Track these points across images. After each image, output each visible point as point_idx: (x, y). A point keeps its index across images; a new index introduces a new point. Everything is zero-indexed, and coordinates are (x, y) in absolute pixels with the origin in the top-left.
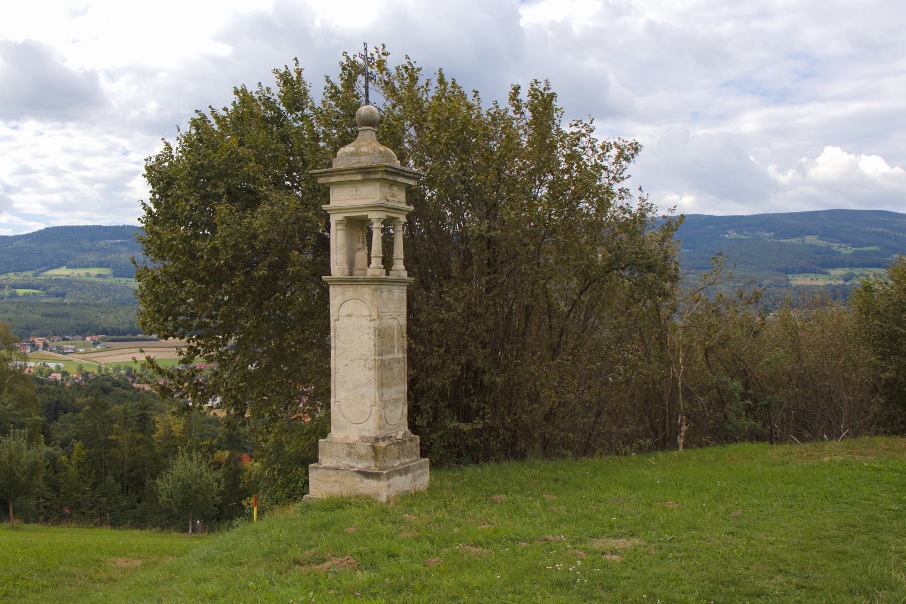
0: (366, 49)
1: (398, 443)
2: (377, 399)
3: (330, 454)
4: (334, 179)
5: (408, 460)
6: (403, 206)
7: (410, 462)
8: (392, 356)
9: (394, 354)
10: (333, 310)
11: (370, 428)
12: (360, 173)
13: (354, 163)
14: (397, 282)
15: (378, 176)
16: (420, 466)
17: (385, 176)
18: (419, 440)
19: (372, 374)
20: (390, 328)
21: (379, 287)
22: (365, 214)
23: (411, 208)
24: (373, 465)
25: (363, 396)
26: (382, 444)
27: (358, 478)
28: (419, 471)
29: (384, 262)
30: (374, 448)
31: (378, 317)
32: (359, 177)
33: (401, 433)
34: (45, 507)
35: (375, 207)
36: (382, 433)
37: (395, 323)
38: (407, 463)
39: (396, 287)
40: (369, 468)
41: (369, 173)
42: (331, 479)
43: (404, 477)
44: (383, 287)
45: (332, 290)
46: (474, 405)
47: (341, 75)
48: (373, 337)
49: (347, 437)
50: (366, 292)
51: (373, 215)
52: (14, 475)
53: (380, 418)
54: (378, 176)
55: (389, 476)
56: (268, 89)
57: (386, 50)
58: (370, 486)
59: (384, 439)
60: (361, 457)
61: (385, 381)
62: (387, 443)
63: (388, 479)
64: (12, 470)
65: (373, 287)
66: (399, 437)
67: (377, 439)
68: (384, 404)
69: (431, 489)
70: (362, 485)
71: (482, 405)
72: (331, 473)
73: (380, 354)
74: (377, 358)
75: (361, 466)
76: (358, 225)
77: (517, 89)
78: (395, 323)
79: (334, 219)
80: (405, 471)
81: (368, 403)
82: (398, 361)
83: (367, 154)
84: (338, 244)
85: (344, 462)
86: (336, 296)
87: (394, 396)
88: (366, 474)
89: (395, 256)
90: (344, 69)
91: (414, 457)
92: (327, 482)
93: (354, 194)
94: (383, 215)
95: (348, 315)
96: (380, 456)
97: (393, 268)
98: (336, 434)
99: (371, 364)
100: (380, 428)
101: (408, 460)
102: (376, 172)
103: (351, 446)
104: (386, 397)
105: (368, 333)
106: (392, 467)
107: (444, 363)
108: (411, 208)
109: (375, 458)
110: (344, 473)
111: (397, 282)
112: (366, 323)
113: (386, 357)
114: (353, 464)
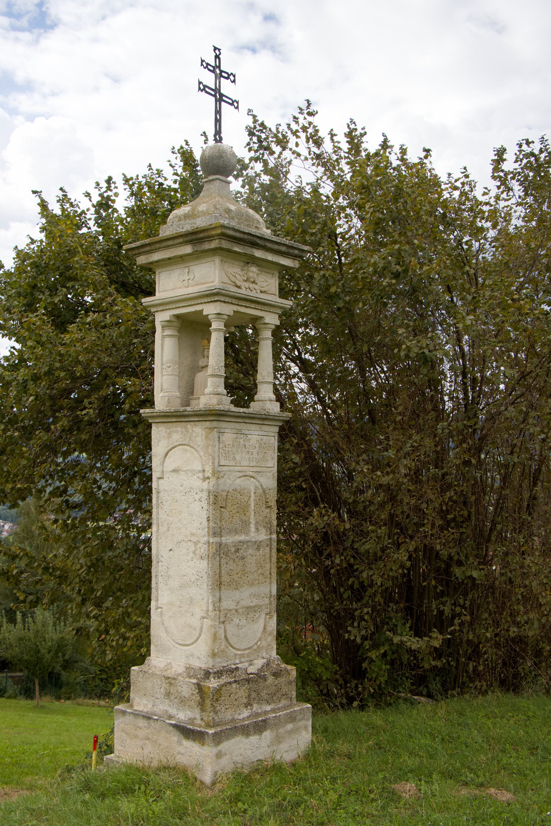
0: (217, 57)
1: (248, 681)
2: (211, 608)
3: (147, 688)
4: (156, 257)
5: (268, 708)
6: (275, 299)
7: (273, 711)
8: (243, 537)
9: (247, 533)
10: (155, 463)
11: (200, 656)
12: (190, 242)
13: (187, 227)
14: (264, 419)
15: (214, 245)
16: (292, 718)
17: (225, 244)
18: (294, 673)
19: (204, 565)
20: (241, 492)
21: (215, 424)
22: (198, 308)
23: (288, 303)
24: (198, 717)
25: (191, 601)
26: (213, 683)
27: (175, 737)
28: (290, 726)
29: (231, 388)
30: (200, 688)
31: (214, 474)
32: (188, 249)
33: (259, 663)
34: (102, 680)
35: (213, 296)
36: (220, 663)
37: (251, 485)
38: (266, 713)
39: (253, 427)
40: (192, 721)
41: (201, 241)
42: (142, 733)
43: (254, 739)
44: (224, 425)
45: (155, 431)
46: (447, 610)
47: (248, 144)
48: (206, 507)
49: (169, 666)
50: (198, 431)
51: (209, 310)
52: (39, 651)
53: (215, 637)
54: (214, 245)
55: (218, 738)
56: (159, 173)
57: (312, 108)
58: (189, 753)
59: (219, 674)
60: (183, 702)
61: (225, 578)
62: (224, 679)
63: (218, 743)
64: (37, 646)
65: (208, 424)
66: (252, 669)
67: (207, 674)
68: (223, 616)
69: (311, 756)
70: (181, 749)
71: (458, 609)
72: (142, 723)
73: (217, 532)
74: (211, 540)
75: (182, 716)
76: (193, 328)
77: (501, 153)
78: (251, 485)
79: (161, 318)
80: (259, 727)
81: (199, 612)
82: (258, 545)
83: (204, 213)
84: (165, 359)
85: (163, 706)
86: (161, 438)
87: (244, 603)
88: (187, 732)
89: (259, 378)
90: (251, 134)
91: (284, 702)
92: (136, 736)
93: (186, 277)
94: (228, 310)
95: (175, 471)
96: (208, 702)
97: (256, 397)
98: (157, 660)
99: (203, 549)
100: (214, 655)
101: (268, 708)
102: (210, 238)
103: (170, 681)
104: (225, 604)
105: (200, 500)
106: (233, 720)
107: (383, 550)
108: (288, 303)
109: (202, 705)
110: (157, 725)
111: (264, 419)
112: (197, 483)
113: (228, 539)
114: (173, 711)
